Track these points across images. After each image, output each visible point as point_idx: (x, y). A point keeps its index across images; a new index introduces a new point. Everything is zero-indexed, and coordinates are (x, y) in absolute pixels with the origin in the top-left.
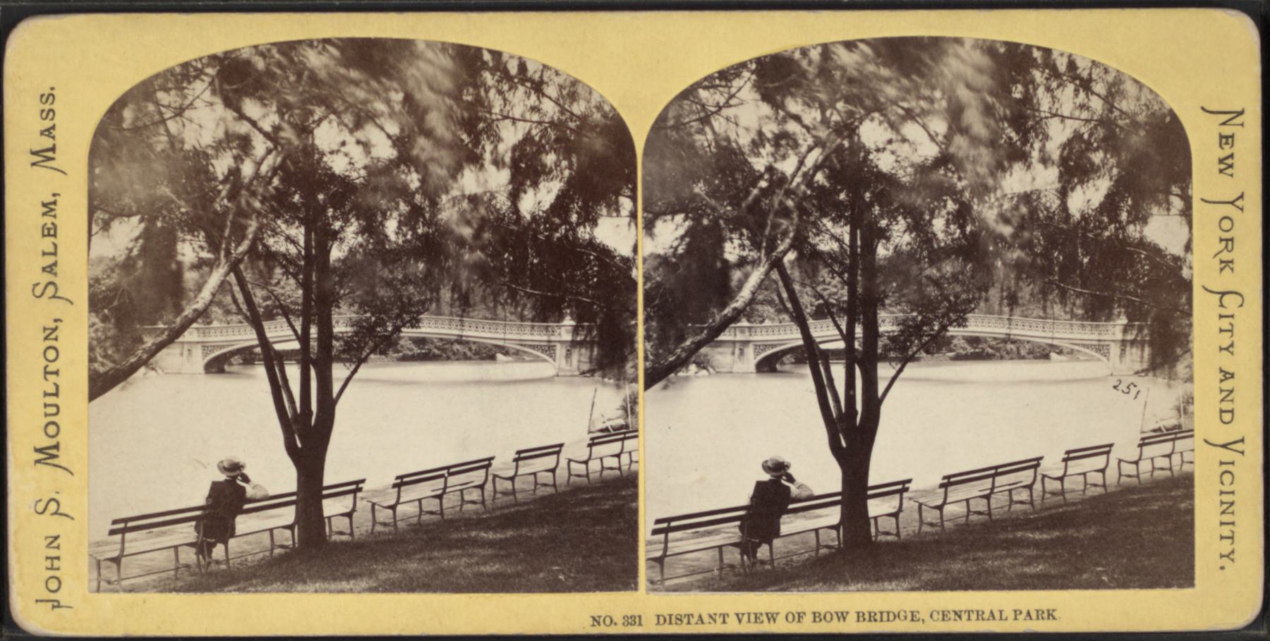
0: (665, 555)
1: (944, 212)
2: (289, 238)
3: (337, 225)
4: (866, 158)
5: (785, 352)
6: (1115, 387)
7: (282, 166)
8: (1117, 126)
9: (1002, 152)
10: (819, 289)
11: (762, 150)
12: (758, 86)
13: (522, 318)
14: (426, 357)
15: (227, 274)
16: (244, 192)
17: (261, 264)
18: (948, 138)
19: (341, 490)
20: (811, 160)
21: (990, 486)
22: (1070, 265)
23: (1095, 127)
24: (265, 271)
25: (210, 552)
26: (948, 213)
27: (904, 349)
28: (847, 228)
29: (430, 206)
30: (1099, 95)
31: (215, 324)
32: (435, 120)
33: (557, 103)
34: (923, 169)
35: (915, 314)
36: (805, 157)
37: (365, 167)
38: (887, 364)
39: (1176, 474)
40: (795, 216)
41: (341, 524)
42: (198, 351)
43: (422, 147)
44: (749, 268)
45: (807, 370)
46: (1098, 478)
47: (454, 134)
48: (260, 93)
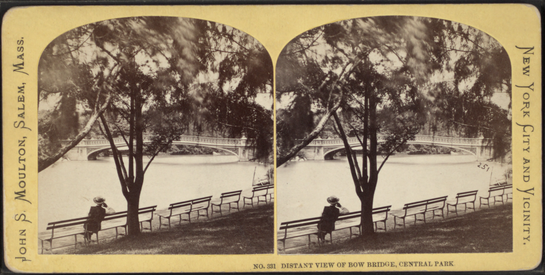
0: (285, 238)
1: (405, 91)
2: (124, 102)
3: (145, 96)
4: (371, 68)
5: (337, 151)
6: (478, 166)
7: (121, 71)
8: (479, 54)
9: (430, 65)
10: (351, 124)
11: (327, 64)
12: (325, 37)
13: (224, 136)
14: (183, 153)
15: (97, 118)
16: (105, 82)
17: (112, 113)
18: (407, 59)
19: (146, 210)
20: (348, 69)
21: (425, 209)
22: (459, 113)
23: (470, 54)
24: (114, 116)
25: (90, 237)
26: (407, 92)
27: (388, 150)
28: (364, 98)
29: (185, 88)
30: (471, 41)
31: (92, 139)
32: (187, 52)
33: (239, 44)
34: (396, 73)
35: (393, 135)
36: (345, 67)
37: (157, 72)
38: (381, 156)
39: (505, 203)
40: (341, 93)
41: (146, 225)
42: (85, 151)
43: (181, 63)
44: (321, 115)
45: (346, 159)
46: (471, 205)
47: (195, 57)
48: (112, 40)
